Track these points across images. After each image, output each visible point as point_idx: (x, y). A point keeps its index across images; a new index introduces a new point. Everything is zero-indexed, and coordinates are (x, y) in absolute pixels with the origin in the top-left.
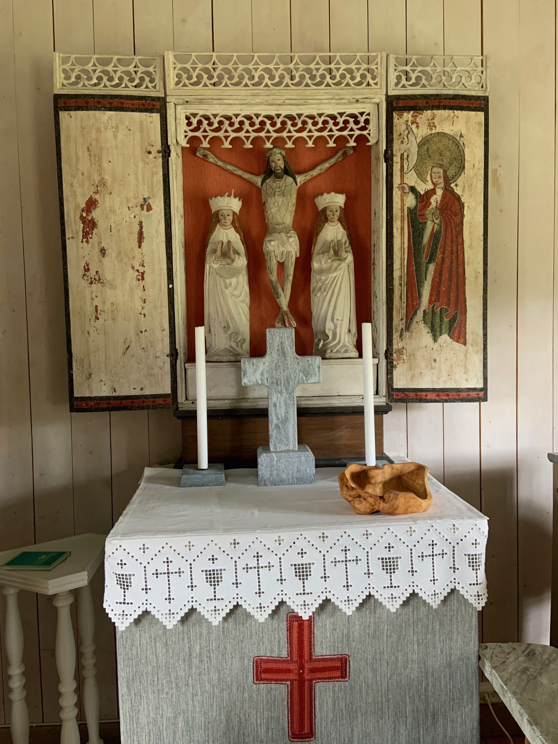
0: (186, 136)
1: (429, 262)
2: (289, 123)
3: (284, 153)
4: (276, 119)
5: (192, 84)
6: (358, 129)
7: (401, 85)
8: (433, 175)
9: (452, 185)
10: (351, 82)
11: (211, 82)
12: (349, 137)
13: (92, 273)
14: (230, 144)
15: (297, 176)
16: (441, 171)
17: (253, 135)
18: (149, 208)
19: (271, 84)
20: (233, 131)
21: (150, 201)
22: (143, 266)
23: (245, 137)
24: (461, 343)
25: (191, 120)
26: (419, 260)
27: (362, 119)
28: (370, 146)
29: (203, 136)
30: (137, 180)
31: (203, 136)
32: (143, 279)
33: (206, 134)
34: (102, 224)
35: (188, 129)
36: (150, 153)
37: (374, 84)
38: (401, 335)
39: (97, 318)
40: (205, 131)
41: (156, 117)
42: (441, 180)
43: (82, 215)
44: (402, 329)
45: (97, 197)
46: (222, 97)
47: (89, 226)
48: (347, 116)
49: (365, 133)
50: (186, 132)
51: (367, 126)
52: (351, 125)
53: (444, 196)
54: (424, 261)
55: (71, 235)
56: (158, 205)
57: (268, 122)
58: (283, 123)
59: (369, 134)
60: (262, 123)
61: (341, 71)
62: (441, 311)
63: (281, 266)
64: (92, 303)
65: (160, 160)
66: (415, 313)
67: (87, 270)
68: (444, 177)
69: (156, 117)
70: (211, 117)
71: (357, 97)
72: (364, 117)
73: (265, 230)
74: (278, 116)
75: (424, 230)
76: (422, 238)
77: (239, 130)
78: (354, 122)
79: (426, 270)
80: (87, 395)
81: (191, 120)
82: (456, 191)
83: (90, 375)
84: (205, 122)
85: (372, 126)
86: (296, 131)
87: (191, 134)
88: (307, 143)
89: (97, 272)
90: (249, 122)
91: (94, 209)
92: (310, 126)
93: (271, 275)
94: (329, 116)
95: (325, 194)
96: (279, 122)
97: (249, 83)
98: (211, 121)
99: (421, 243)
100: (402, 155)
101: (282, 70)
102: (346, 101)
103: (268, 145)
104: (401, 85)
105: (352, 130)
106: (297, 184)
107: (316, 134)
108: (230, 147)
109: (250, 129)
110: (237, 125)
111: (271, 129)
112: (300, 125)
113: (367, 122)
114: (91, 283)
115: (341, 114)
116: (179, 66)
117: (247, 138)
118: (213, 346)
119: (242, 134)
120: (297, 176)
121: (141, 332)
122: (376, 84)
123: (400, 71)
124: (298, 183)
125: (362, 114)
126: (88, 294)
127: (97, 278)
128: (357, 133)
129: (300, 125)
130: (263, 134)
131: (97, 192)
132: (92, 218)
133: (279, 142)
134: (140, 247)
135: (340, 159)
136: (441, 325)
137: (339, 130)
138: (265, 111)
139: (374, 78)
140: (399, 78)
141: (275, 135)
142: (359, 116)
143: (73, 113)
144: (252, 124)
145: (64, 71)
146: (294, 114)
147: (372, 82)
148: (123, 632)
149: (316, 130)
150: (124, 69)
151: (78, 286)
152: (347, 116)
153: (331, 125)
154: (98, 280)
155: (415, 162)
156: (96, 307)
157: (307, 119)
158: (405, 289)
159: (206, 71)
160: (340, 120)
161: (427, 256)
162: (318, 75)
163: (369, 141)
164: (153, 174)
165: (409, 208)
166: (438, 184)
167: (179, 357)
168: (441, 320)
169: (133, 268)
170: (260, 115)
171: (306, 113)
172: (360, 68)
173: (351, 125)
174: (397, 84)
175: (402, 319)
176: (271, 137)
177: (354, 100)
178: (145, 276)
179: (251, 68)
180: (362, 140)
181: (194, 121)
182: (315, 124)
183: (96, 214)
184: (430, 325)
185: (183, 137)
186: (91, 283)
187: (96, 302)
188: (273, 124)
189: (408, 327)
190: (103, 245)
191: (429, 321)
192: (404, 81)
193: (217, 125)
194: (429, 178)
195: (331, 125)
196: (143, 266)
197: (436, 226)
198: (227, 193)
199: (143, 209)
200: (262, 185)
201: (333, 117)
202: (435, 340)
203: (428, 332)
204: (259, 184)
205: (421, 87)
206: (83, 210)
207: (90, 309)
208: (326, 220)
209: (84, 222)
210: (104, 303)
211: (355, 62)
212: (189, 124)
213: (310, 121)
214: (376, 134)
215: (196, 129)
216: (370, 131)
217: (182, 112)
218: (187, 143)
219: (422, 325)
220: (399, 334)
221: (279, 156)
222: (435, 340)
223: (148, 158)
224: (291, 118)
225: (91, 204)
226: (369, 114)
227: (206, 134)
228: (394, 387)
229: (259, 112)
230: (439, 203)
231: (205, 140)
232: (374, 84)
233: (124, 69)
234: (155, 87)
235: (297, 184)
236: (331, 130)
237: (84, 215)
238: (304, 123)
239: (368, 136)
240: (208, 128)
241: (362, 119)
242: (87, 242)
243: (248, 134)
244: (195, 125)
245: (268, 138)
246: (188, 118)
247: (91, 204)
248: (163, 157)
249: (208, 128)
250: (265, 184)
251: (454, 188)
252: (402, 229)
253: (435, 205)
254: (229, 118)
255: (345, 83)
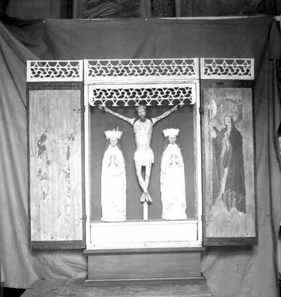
1: (225, 167)
2: (148, 93)
3: (145, 107)
7: (207, 73)
9: (236, 126)
13: (43, 173)
14: (128, 104)
15: (153, 119)
16: (229, 118)
18: (73, 139)
20: (118, 97)
21: (74, 135)
22: (69, 170)
27: (187, 91)
28: (192, 105)
29: (103, 101)
30: (68, 125)
31: (103, 101)
32: (69, 177)
34: (48, 148)
35: (94, 97)
36: (75, 110)
38: (210, 207)
39: (44, 198)
40: (104, 98)
41: (79, 92)
42: (230, 124)
43: (38, 144)
45: (47, 134)
47: (42, 149)
49: (189, 98)
53: (232, 132)
55: (32, 154)
56: (78, 137)
58: (145, 93)
59: (191, 99)
63: (144, 168)
64: (41, 190)
65: (80, 114)
66: (218, 196)
67: (40, 172)
69: (79, 92)
72: (188, 90)
74: (143, 89)
77: (122, 97)
80: (38, 240)
83: (40, 229)
84: (104, 93)
85: (193, 95)
87: (96, 99)
88: (158, 103)
89: (45, 173)
91: (45, 140)
92: (159, 94)
94: (169, 89)
96: (153, 92)
97: (127, 74)
103: (137, 104)
104: (207, 73)
105: (182, 96)
106: (152, 123)
108: (117, 106)
109: (128, 96)
110: (120, 95)
113: (190, 92)
114: (42, 179)
115: (176, 88)
116: (91, 66)
117: (126, 101)
119: (123, 99)
121: (67, 206)
125: (187, 88)
126: (40, 185)
127: (45, 177)
130: (134, 99)
131: (46, 132)
132: (44, 145)
133: (143, 103)
134: (68, 159)
135: (176, 109)
137: (164, 97)
139: (193, 71)
140: (206, 70)
141: (141, 99)
143: (36, 91)
144: (129, 94)
145: (32, 70)
146: (151, 88)
147: (191, 73)
148: (275, 19)
150: (62, 67)
151: (35, 181)
152: (179, 89)
154: (46, 178)
156: (44, 192)
157: (158, 91)
160: (176, 91)
162: (163, 69)
164: (76, 121)
165: (213, 138)
168: (232, 199)
169: (64, 171)
171: (157, 88)
173: (181, 94)
174: (205, 73)
178: (70, 175)
180: (188, 102)
181: (98, 93)
182: (162, 93)
183: (46, 143)
186: (42, 179)
187: (44, 190)
189: (213, 203)
190: (49, 159)
191: (225, 200)
192: (209, 72)
194: (223, 122)
195: (170, 94)
196: (69, 170)
199: (70, 140)
200: (134, 123)
204: (132, 123)
206: (39, 141)
207: (40, 194)
208: (169, 142)
209: (39, 147)
210: (48, 190)
212: (95, 94)
213: (159, 92)
214: (195, 99)
215: (99, 97)
219: (221, 202)
223: (73, 113)
224: (149, 90)
225: (43, 138)
226: (191, 89)
233: (62, 67)
234: (78, 76)
236: (171, 97)
237: (40, 143)
240: (105, 96)
241: (187, 91)
242: (41, 158)
244: (98, 94)
245: (137, 101)
246: (94, 91)
247: (43, 138)
248: (81, 112)
249: (105, 96)
250: (135, 124)
252: (210, 149)
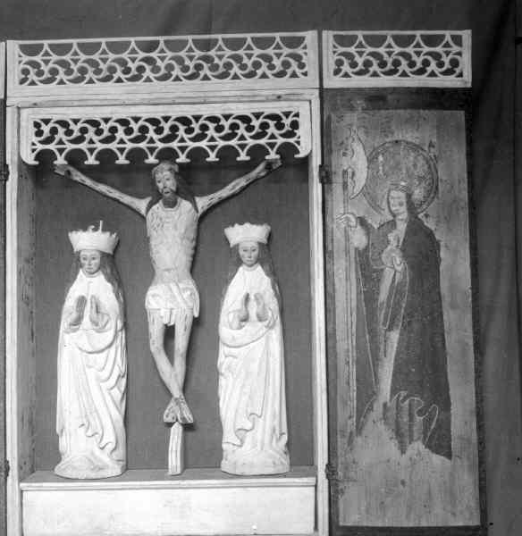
0: (33, 150)
1: (390, 329)
4: (163, 124)
5: (386, 73)
6: (282, 135)
8: (392, 202)
9: (420, 216)
10: (269, 73)
11: (383, 70)
12: (268, 147)
16: (402, 195)
17: (129, 146)
19: (411, 72)
23: (118, 149)
24: (444, 455)
25: (42, 128)
26: (374, 325)
27: (287, 122)
33: (62, 148)
35: (36, 139)
37: (303, 74)
38: (350, 442)
42: (404, 209)
44: (351, 433)
46: (85, 97)
48: (265, 117)
49: (292, 140)
50: (33, 144)
51: (296, 131)
52: (272, 130)
54: (382, 328)
57: (151, 128)
59: (298, 143)
60: (144, 130)
61: (254, 59)
62: (410, 405)
63: (169, 332)
68: (407, 202)
70: (71, 123)
71: (279, 93)
73: (147, 273)
74: (166, 119)
75: (379, 280)
76: (378, 294)
78: (276, 125)
79: (385, 341)
81: (42, 128)
82: (426, 224)
86: (191, 139)
87: (40, 147)
90: (124, 128)
93: (191, 304)
94: (239, 117)
95: (236, 225)
98: (70, 128)
99: (377, 300)
100: (345, 172)
101: (170, 59)
102: (263, 98)
103: (151, 160)
105: (273, 137)
107: (221, 143)
111: (156, 137)
112: (197, 131)
113: (295, 125)
115: (257, 116)
116: (26, 58)
118: (68, 452)
120: (197, 199)
122: (305, 74)
123: (340, 54)
124: (199, 208)
125: (287, 114)
128: (280, 140)
129: (197, 131)
135: (263, 174)
136: (410, 426)
138: (146, 112)
139: (302, 66)
141: (161, 145)
142: (284, 117)
147: (299, 72)
149: (220, 138)
152: (265, 117)
153: (242, 131)
155: (363, 182)
157: (207, 123)
158: (355, 370)
159: (63, 64)
160: (256, 123)
161: (385, 319)
163: (298, 152)
165: (356, 249)
166: (398, 214)
167: (10, 473)
170: (170, 117)
172: (281, 54)
173: (272, 130)
174: (337, 72)
175: (350, 417)
176: (156, 148)
177: (275, 98)
179: (111, 54)
180: (288, 151)
181: (46, 129)
182: (219, 129)
184: (394, 427)
185: (30, 152)
188: (159, 131)
189: (359, 429)
191: (392, 421)
193: (79, 134)
194: (384, 204)
197: (398, 274)
198: (93, 227)
200: (147, 213)
201: (245, 119)
202: (403, 452)
203: (391, 438)
205: (400, 76)
208: (239, 262)
211: (274, 46)
212: (39, 133)
213: (212, 126)
215: (48, 141)
216: (299, 137)
217: (28, 118)
218: (36, 159)
219: (381, 427)
220: (346, 440)
221: (167, 174)
222: (403, 452)
224: (184, 121)
226: (297, 115)
227: (62, 148)
228: (341, 524)
229: (139, 115)
230: (401, 240)
231: (61, 154)
232: (303, 74)
235: (197, 212)
236: (242, 138)
238: (204, 128)
239: (296, 145)
241: (287, 122)
243: (123, 145)
246: (37, 125)
250: (150, 212)
251: (424, 219)
253: (395, 244)
254: (94, 123)
255: (145, 77)
